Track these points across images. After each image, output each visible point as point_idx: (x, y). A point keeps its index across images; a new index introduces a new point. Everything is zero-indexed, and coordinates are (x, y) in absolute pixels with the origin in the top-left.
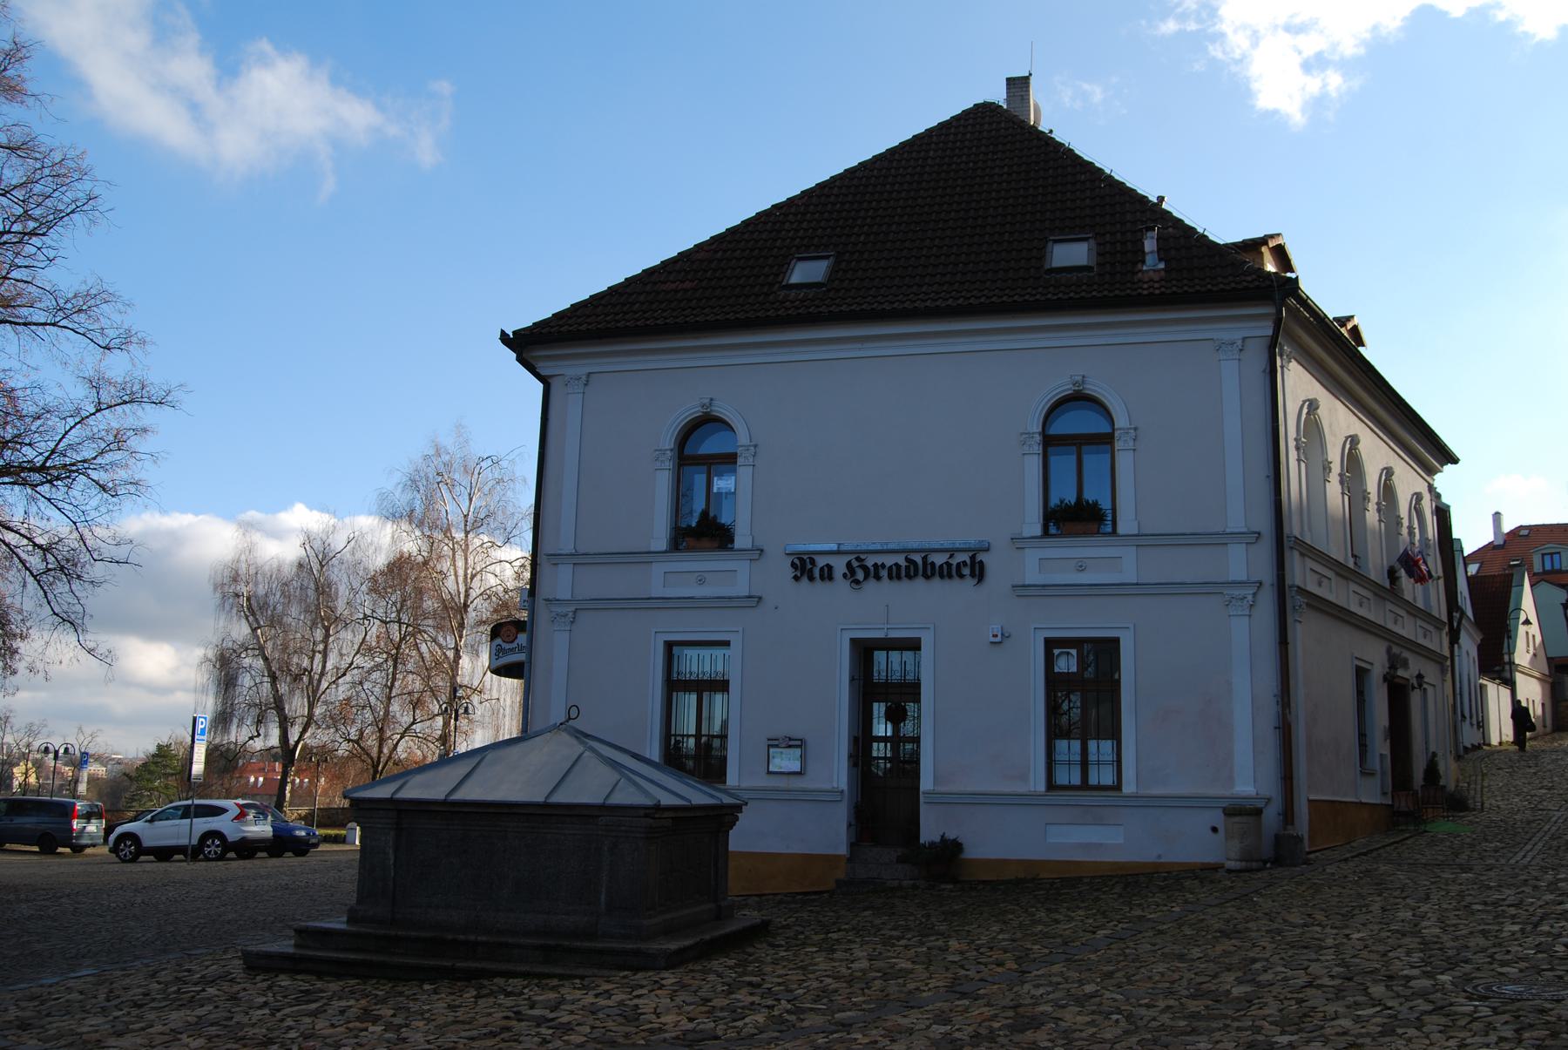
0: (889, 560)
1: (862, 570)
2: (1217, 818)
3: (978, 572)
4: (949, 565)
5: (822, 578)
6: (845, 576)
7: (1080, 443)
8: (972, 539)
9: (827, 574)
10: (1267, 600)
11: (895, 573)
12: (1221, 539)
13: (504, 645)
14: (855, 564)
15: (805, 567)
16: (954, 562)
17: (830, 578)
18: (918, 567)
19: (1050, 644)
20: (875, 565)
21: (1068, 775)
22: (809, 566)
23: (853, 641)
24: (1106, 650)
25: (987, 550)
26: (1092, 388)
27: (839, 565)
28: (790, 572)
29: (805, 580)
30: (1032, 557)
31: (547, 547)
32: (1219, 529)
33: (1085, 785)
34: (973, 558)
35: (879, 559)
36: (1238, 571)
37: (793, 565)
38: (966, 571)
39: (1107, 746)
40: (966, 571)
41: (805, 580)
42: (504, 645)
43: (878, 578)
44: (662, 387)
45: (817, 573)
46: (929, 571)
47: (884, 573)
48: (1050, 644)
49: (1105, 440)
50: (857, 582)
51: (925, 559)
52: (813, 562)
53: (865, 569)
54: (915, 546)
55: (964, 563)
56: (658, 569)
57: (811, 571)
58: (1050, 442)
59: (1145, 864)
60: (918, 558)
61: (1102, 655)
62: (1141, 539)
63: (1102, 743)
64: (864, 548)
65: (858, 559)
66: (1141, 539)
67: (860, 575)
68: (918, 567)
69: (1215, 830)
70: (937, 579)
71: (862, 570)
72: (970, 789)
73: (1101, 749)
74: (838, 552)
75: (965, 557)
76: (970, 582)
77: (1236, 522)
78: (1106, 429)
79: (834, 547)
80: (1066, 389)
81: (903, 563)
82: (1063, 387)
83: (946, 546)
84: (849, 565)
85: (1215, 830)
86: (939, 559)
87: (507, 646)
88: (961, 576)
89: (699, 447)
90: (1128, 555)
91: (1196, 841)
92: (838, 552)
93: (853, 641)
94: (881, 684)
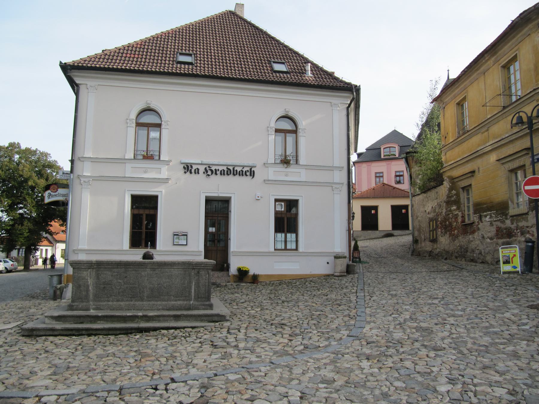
0: (221, 168)
1: (210, 171)
2: (331, 259)
3: (252, 174)
4: (242, 171)
5: (195, 173)
6: (204, 173)
7: (148, 126)
8: (250, 163)
9: (197, 171)
10: (345, 188)
11: (222, 173)
12: (331, 168)
13: (52, 193)
14: (208, 169)
15: (188, 168)
16: (244, 170)
17: (198, 173)
18: (230, 171)
19: (276, 200)
20: (216, 170)
21: (280, 246)
22: (190, 168)
23: (230, 198)
24: (292, 204)
25: (255, 167)
26: (152, 106)
27: (202, 169)
28: (183, 171)
29: (188, 173)
30: (271, 170)
31: (78, 154)
32: (331, 165)
33: (286, 249)
34: (251, 169)
35: (217, 168)
36: (337, 180)
37: (184, 167)
38: (248, 174)
39: (294, 235)
40: (248, 174)
41: (188, 173)
42: (52, 193)
43: (216, 174)
44: (129, 96)
45: (193, 171)
46: (235, 173)
47: (218, 173)
48: (276, 200)
49: (158, 126)
50: (209, 175)
51: (234, 168)
52: (192, 167)
53: (212, 171)
54: (230, 164)
55: (248, 171)
56: (129, 166)
57: (191, 170)
58: (139, 125)
59: (306, 275)
60: (231, 168)
61: (292, 204)
62: (309, 167)
63: (289, 235)
64: (211, 163)
65: (209, 167)
66: (309, 167)
67: (209, 173)
68: (230, 171)
69: (328, 263)
70: (237, 176)
71: (210, 171)
72: (100, 249)
73: (291, 237)
74: (202, 164)
75: (248, 169)
76: (249, 178)
77: (336, 164)
78: (159, 122)
79: (200, 162)
80: (283, 114)
81: (226, 170)
82: (141, 106)
83: (241, 164)
84: (206, 169)
85: (328, 263)
86: (239, 169)
87: (53, 194)
88: (247, 175)
89: (148, 121)
90: (303, 171)
91: (320, 267)
92: (202, 164)
93: (230, 198)
94: (218, 212)
